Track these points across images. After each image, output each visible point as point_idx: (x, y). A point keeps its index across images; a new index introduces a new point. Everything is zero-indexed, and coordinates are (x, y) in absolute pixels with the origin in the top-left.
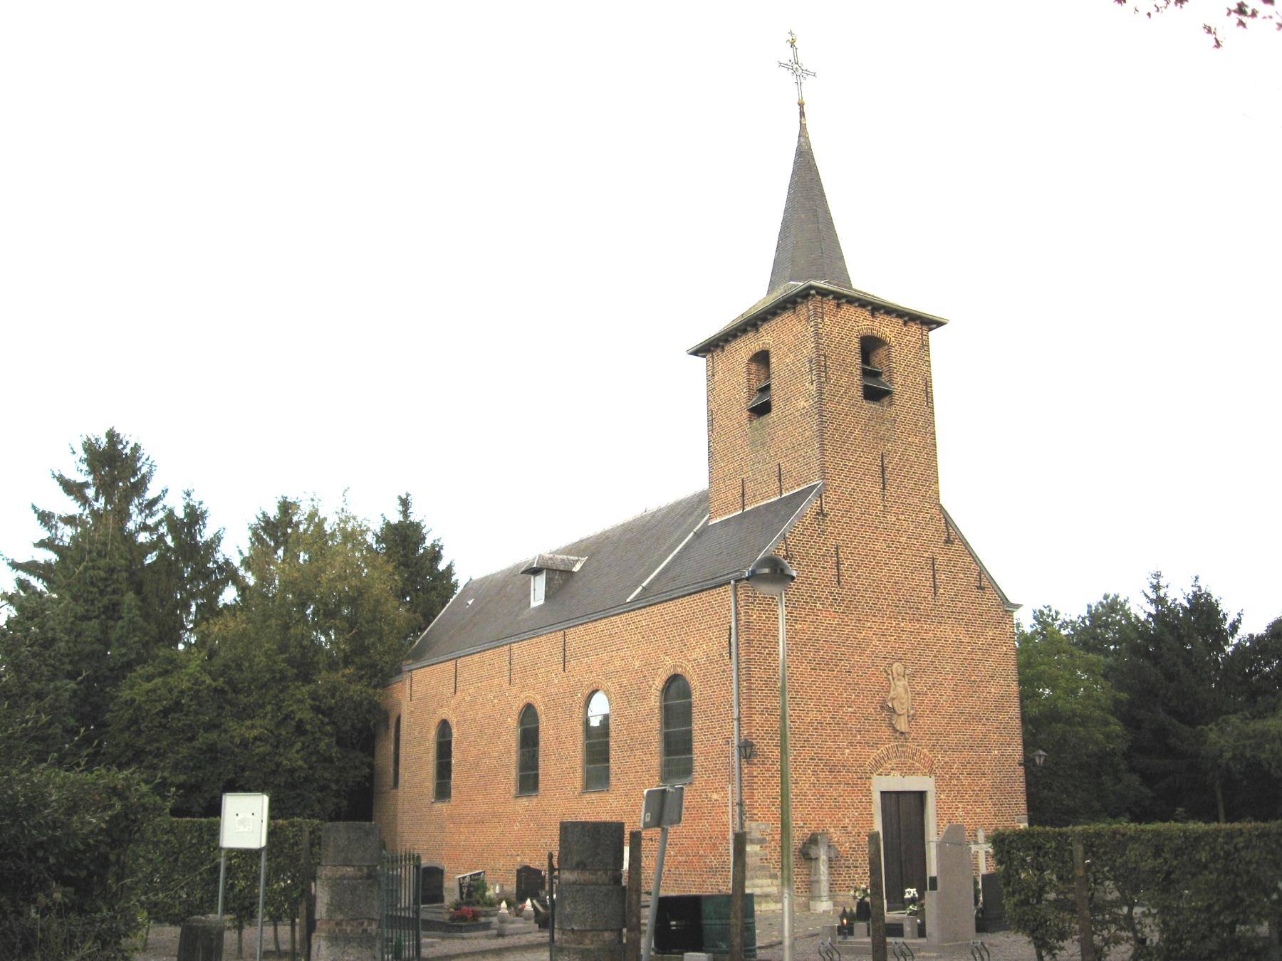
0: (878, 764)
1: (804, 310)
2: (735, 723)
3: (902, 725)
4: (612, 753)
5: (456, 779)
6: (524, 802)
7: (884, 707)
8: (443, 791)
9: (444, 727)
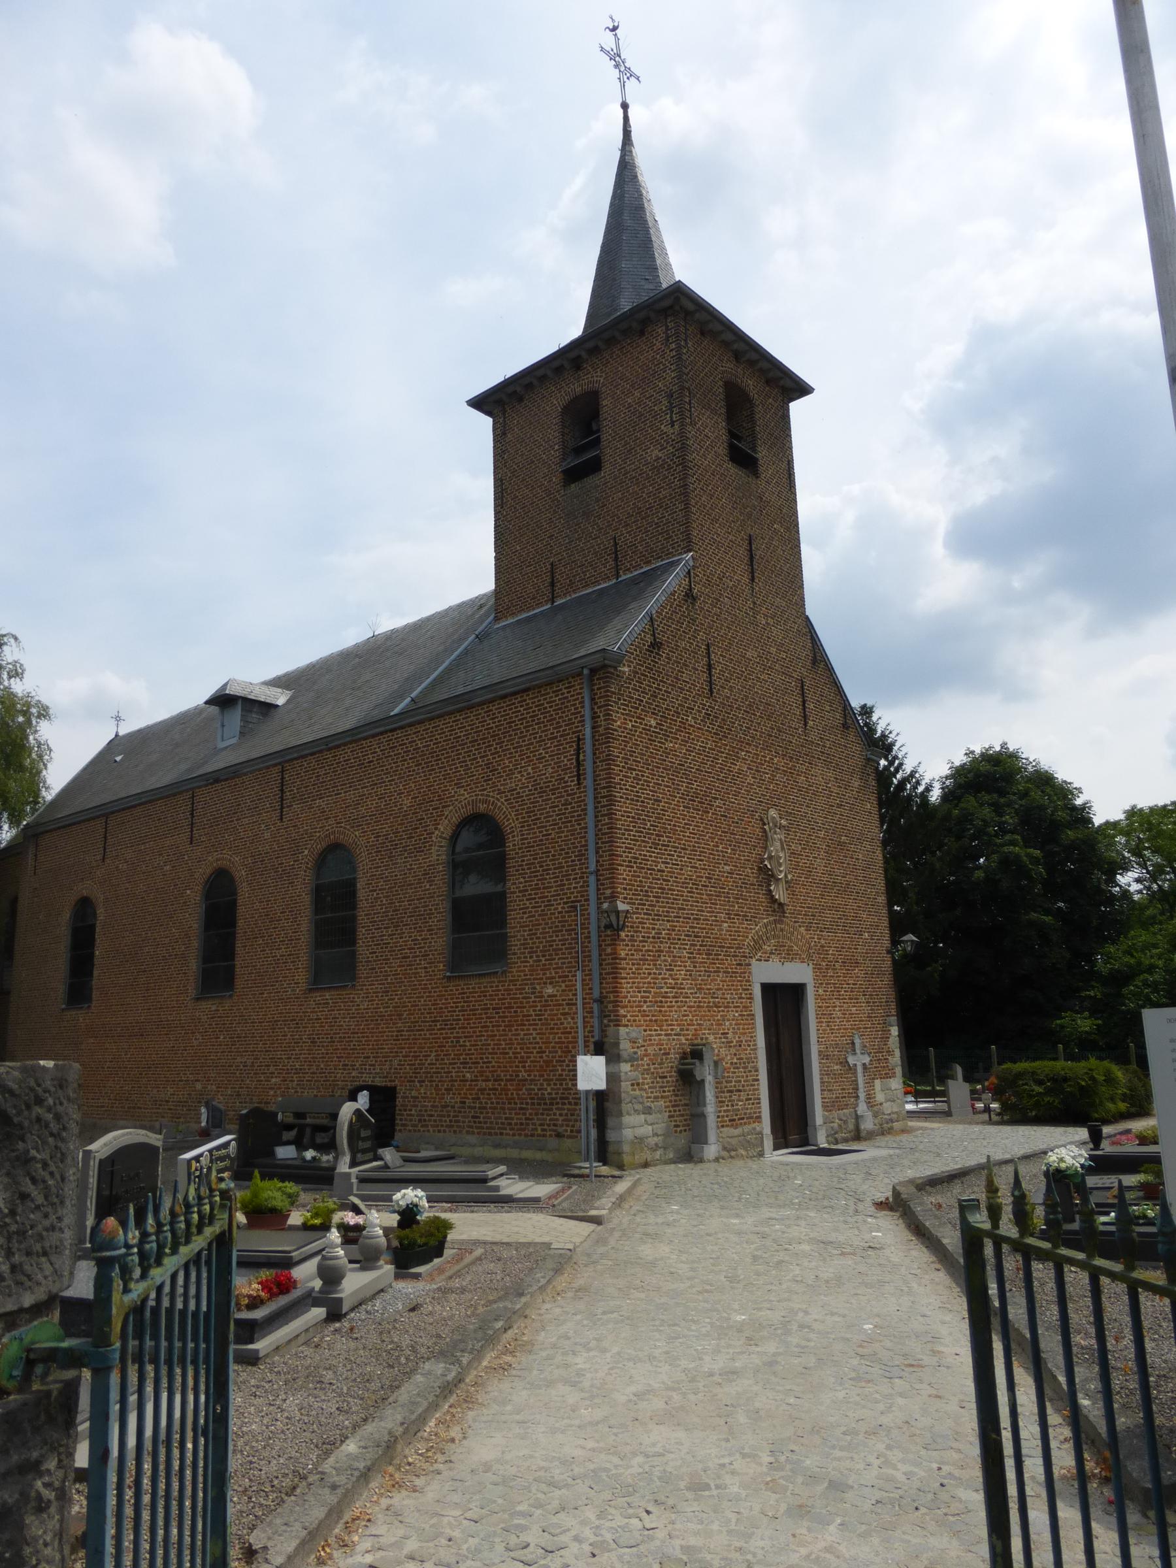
0: (757, 946)
1: (661, 330)
2: (592, 879)
3: (780, 894)
4: (361, 932)
5: (98, 975)
6: (209, 1006)
7: (763, 870)
8: (79, 991)
9: (85, 906)
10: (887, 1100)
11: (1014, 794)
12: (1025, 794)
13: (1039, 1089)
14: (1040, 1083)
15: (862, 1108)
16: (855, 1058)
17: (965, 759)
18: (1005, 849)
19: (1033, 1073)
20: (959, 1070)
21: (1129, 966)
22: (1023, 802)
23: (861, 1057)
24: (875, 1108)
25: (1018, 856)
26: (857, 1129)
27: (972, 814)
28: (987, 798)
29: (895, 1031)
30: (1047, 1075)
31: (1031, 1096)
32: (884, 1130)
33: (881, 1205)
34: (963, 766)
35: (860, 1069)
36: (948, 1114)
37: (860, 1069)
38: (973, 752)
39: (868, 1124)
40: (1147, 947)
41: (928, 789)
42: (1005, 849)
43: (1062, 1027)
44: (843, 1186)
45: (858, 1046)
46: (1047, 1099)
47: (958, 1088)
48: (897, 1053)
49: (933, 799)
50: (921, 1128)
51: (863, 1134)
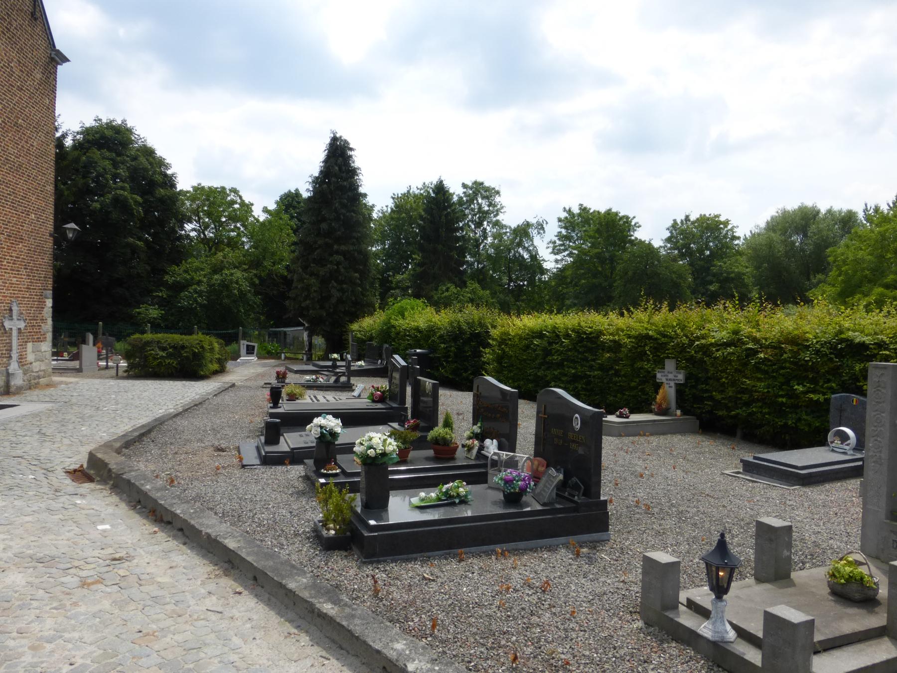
8: (749, 468)
10: (36, 360)
11: (128, 156)
12: (135, 159)
13: (161, 353)
14: (163, 349)
15: (14, 367)
16: (12, 323)
17: (94, 124)
18: (118, 192)
19: (158, 342)
20: (91, 337)
21: (186, 280)
22: (133, 163)
23: (18, 322)
24: (25, 367)
25: (126, 198)
26: (7, 385)
27: (96, 163)
28: (108, 154)
29: (49, 303)
30: (169, 344)
31: (155, 359)
32: (32, 385)
33: (80, 475)
34: (92, 128)
35: (15, 333)
36: (79, 370)
37: (15, 333)
38: (100, 120)
39: (18, 381)
40: (197, 269)
41: (64, 136)
42: (118, 192)
43: (139, 313)
44: (19, 453)
45: (15, 313)
46: (167, 361)
47: (89, 351)
48: (50, 322)
49: (67, 144)
50: (61, 383)
51: (12, 389)
